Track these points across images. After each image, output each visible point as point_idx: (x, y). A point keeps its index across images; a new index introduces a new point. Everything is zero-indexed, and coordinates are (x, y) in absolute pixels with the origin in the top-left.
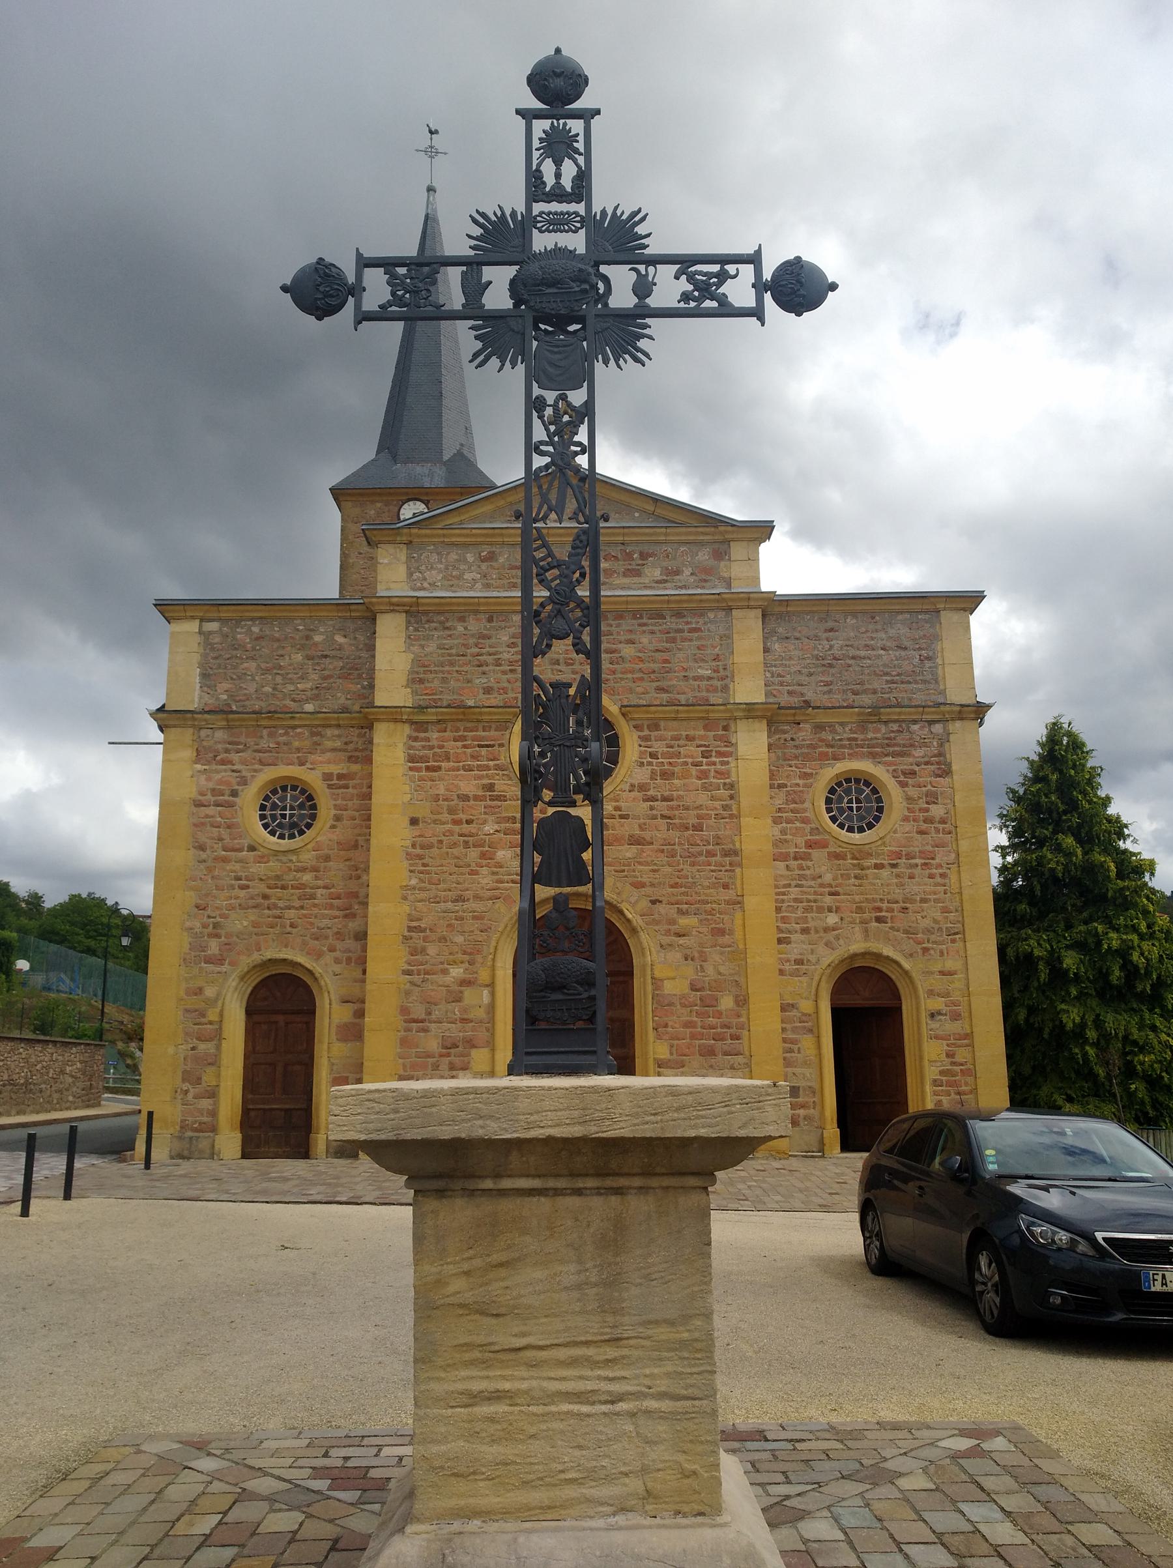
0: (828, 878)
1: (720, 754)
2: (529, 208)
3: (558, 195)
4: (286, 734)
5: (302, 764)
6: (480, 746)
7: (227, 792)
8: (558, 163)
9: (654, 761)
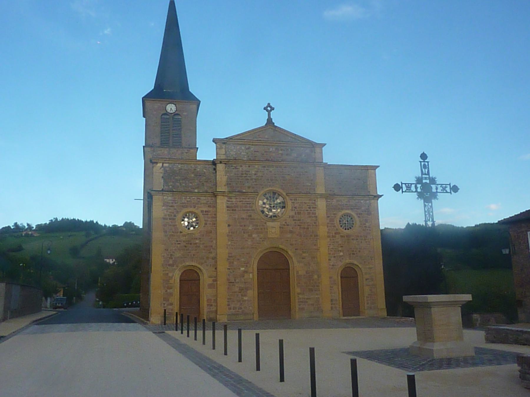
0: (340, 242)
1: (313, 208)
2: (422, 176)
3: (425, 174)
4: (190, 198)
5: (194, 208)
6: (247, 204)
7: (173, 215)
8: (425, 169)
9: (296, 209)
